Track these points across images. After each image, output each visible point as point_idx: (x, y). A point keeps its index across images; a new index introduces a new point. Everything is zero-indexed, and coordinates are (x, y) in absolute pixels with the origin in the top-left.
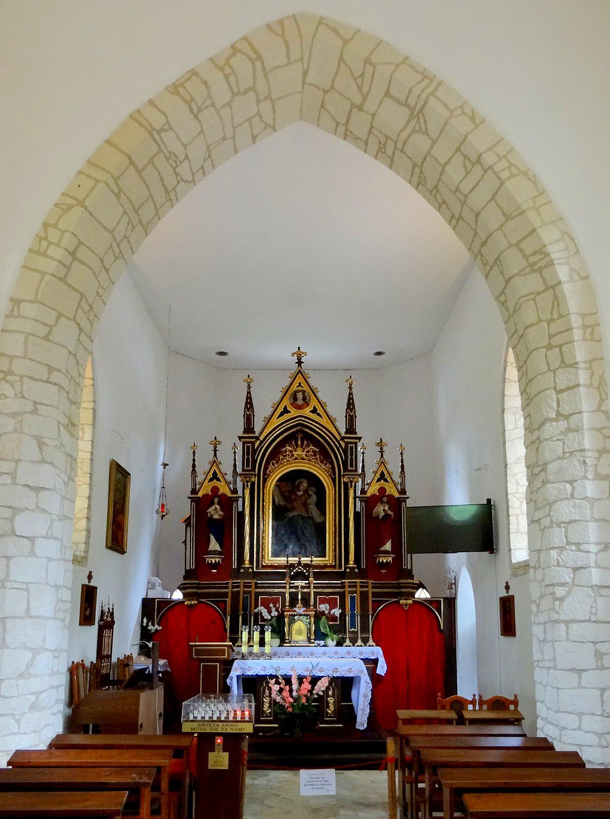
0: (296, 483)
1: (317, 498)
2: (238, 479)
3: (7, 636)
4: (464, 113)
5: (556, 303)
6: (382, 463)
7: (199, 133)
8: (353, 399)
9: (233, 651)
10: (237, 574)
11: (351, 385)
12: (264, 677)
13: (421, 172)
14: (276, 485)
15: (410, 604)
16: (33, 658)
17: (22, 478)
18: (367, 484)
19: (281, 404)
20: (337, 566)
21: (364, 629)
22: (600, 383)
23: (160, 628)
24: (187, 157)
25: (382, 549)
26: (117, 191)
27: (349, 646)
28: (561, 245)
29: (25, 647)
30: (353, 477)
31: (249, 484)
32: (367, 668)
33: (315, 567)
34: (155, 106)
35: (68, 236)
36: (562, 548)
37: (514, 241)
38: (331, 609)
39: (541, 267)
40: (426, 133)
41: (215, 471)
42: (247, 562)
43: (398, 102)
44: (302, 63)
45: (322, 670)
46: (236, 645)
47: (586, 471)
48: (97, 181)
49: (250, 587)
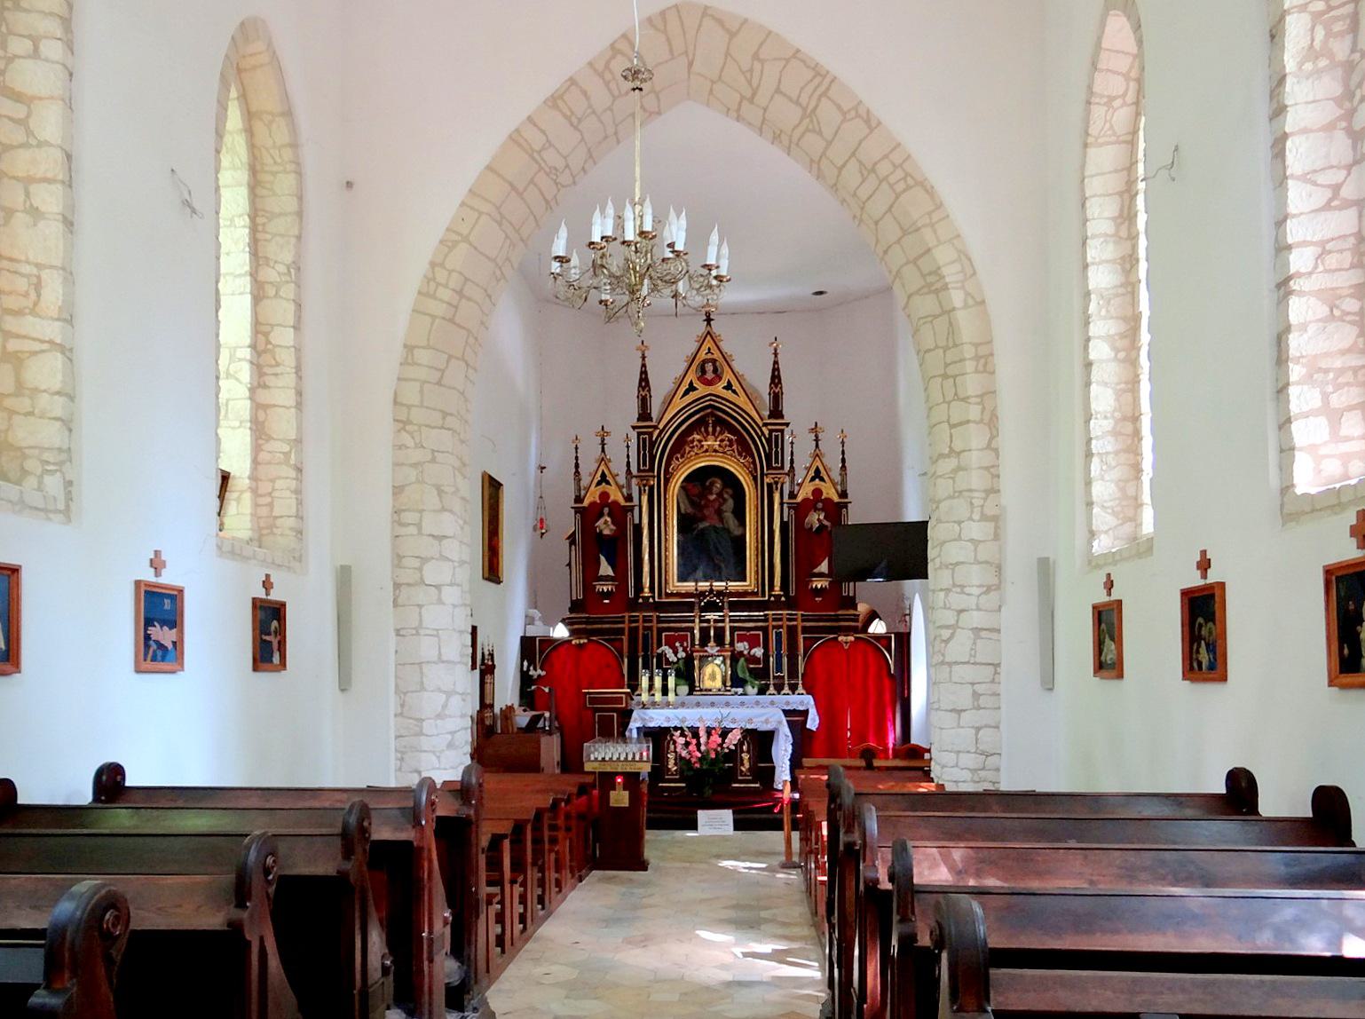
0: (707, 484)
1: (735, 504)
2: (634, 481)
3: (424, 680)
4: (858, 116)
5: (951, 330)
6: (817, 455)
7: (581, 141)
8: (778, 369)
9: (632, 699)
10: (633, 605)
11: (776, 350)
12: (667, 730)
13: (819, 169)
14: (682, 487)
15: (851, 642)
16: (447, 700)
18: (798, 484)
19: (685, 379)
20: (760, 594)
21: (793, 673)
22: (991, 419)
23: (543, 673)
24: (567, 166)
25: (816, 571)
26: (499, 219)
27: (788, 694)
28: (957, 267)
29: (440, 690)
30: (779, 476)
31: (647, 488)
32: (788, 721)
33: (732, 594)
34: (535, 125)
35: (455, 275)
36: (948, 591)
38: (751, 648)
39: (937, 289)
40: (820, 133)
41: (603, 472)
42: (646, 590)
43: (790, 99)
44: (687, 56)
45: (734, 721)
46: (636, 693)
47: (972, 512)
48: (481, 213)
49: (651, 621)
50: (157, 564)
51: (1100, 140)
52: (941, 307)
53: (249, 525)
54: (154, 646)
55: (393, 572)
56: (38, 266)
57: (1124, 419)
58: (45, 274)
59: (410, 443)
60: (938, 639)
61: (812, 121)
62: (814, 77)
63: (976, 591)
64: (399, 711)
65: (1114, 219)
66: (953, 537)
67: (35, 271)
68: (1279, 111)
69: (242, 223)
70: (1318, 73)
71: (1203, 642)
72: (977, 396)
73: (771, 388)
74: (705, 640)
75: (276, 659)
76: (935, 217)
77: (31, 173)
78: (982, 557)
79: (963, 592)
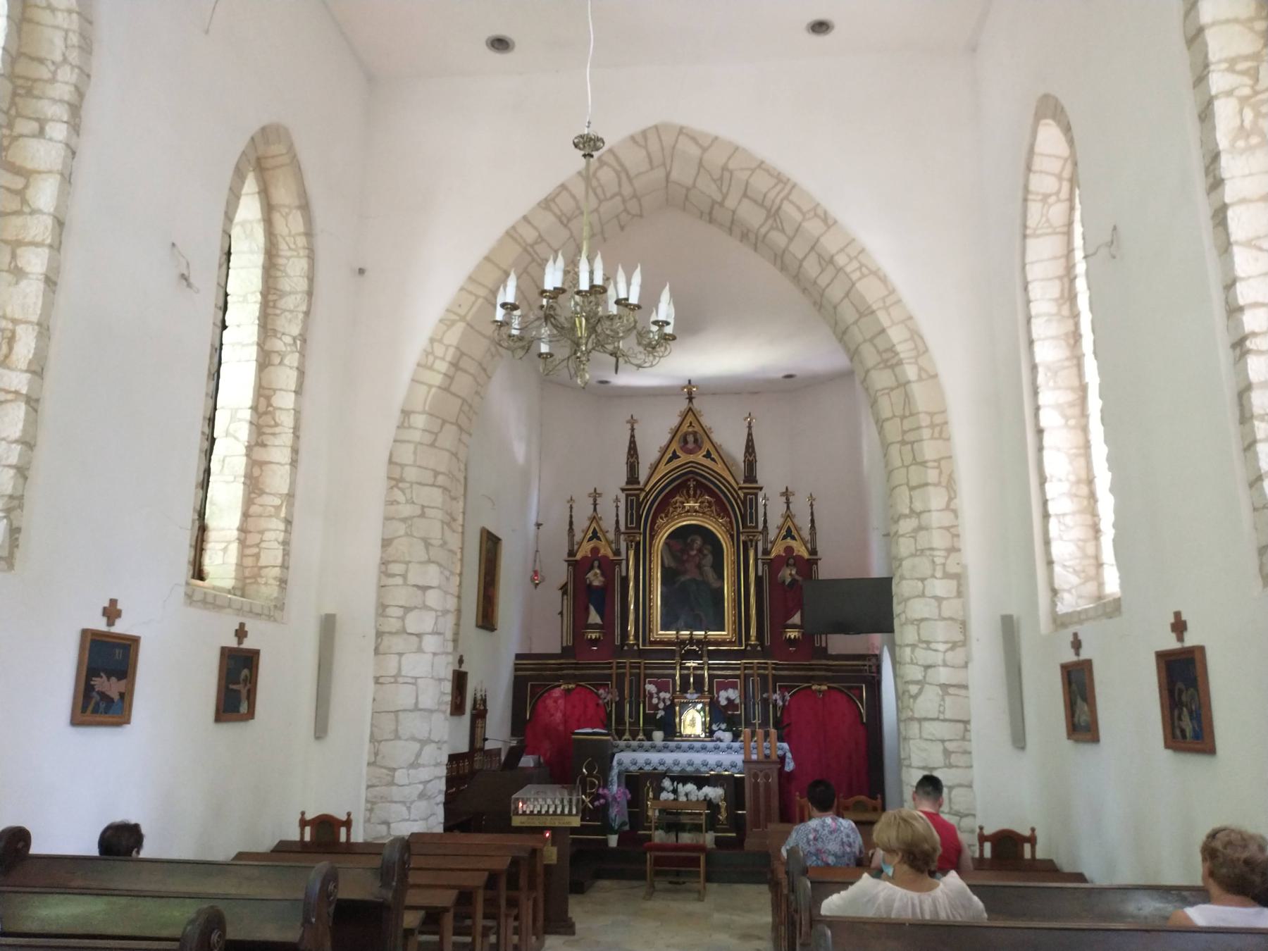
3: (399, 728)
4: (816, 215)
7: (569, 238)
10: (621, 651)
11: (750, 423)
14: (666, 543)
17: (412, 579)
18: (771, 542)
21: (765, 723)
22: (949, 481)
36: (913, 646)
37: (868, 337)
40: (783, 231)
41: (595, 529)
42: (632, 638)
47: (934, 570)
50: (112, 612)
51: (1039, 232)
52: (897, 380)
53: (233, 574)
54: (96, 697)
55: (376, 621)
56: (15, 322)
57: (1078, 482)
58: (20, 330)
59: (401, 498)
60: (907, 694)
61: (775, 220)
62: (776, 185)
63: (942, 647)
64: (373, 759)
65: (1056, 300)
66: (917, 594)
67: (10, 326)
68: (1216, 184)
69: (255, 300)
70: (1250, 149)
71: (1185, 709)
72: (935, 461)
73: (745, 457)
74: (685, 687)
75: (244, 708)
76: (889, 301)
77: (20, 237)
78: (946, 614)
79: (929, 649)
